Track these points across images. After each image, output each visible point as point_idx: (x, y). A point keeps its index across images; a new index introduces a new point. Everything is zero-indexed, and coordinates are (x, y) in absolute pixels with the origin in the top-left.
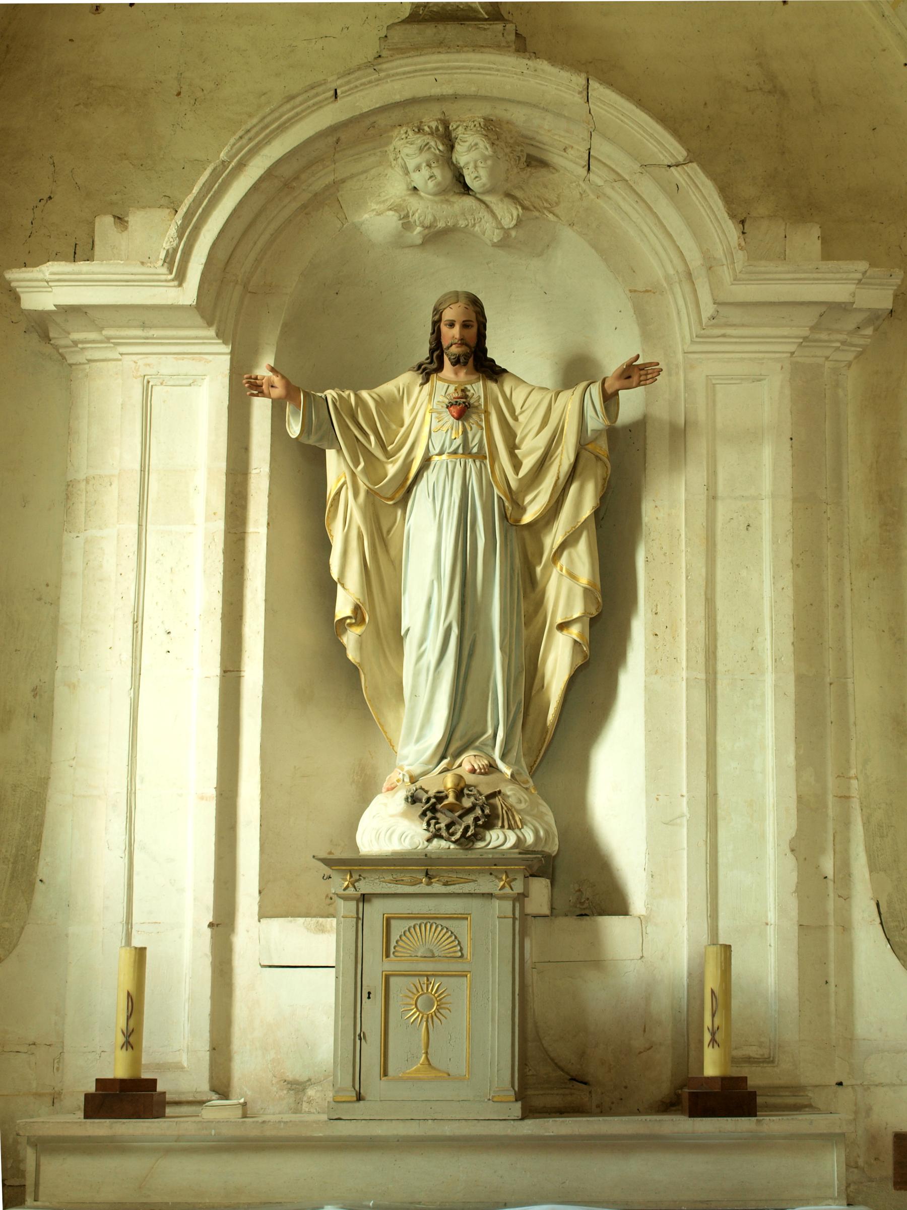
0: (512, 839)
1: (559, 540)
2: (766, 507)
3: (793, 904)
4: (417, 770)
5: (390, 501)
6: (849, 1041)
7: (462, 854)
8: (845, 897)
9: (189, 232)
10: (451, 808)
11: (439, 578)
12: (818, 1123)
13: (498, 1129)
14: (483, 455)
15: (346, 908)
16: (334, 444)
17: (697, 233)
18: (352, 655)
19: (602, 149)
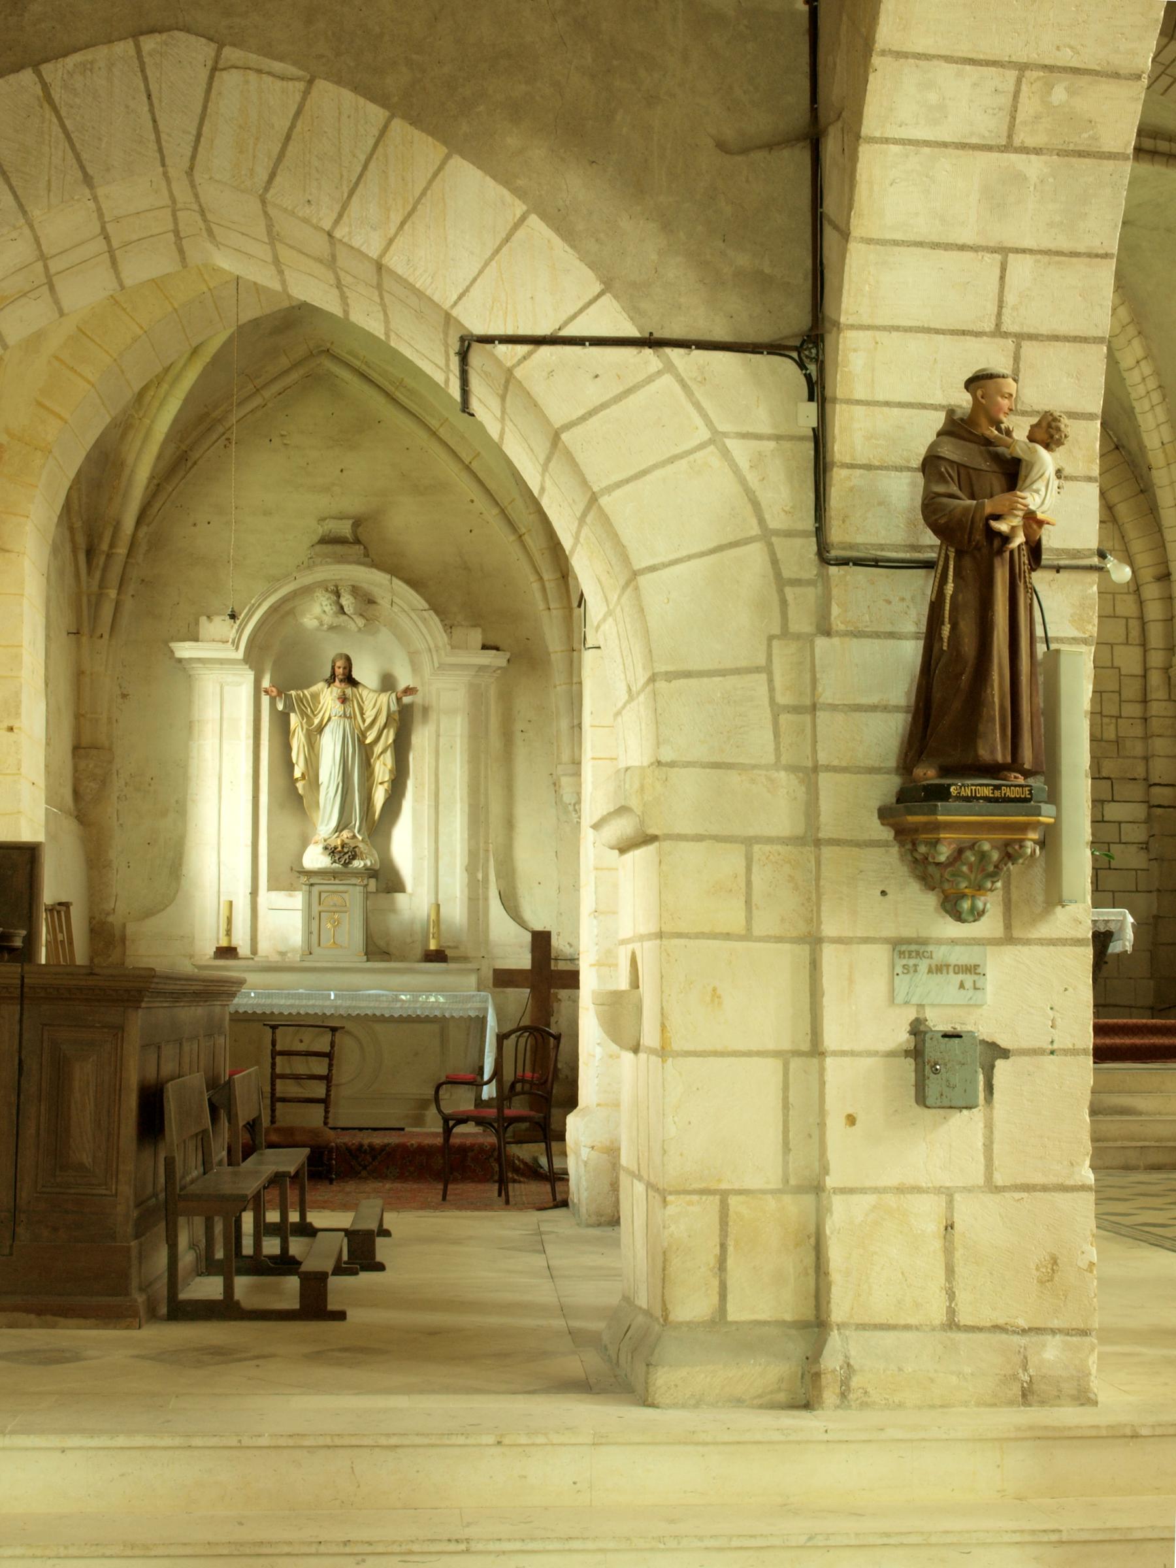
0: (362, 864)
3: (466, 890)
4: (326, 836)
5: (314, 734)
6: (487, 942)
7: (345, 870)
8: (486, 888)
12: (469, 966)
15: (305, 888)
16: (294, 711)
18: (300, 791)
19: (396, 600)
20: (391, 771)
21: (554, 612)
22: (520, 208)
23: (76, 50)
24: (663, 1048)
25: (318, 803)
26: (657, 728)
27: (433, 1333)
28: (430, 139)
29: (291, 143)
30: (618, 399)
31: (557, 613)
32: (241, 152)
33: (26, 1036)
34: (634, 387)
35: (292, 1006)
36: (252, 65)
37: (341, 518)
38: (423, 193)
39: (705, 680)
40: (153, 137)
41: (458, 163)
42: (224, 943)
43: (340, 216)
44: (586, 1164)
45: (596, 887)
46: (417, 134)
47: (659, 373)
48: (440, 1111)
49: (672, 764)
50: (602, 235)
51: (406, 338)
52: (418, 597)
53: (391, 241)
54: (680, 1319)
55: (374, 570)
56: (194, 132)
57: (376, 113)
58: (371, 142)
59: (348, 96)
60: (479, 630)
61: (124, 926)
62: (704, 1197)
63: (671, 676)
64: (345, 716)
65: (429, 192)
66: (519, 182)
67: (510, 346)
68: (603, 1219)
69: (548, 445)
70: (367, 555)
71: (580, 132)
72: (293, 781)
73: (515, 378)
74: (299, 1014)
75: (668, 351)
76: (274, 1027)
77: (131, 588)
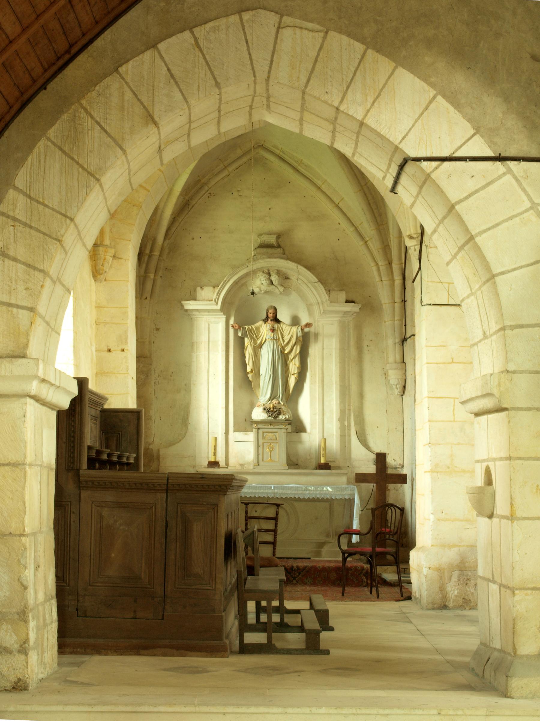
0: (284, 417)
1: (292, 357)
2: (334, 351)
3: (339, 431)
4: (264, 403)
6: (350, 458)
8: (349, 430)
9: (219, 294)
10: (272, 411)
11: (268, 364)
12: (342, 471)
13: (284, 471)
14: (277, 340)
16: (247, 337)
17: (320, 297)
18: (250, 379)
19: (300, 277)
20: (298, 368)
21: (385, 282)
22: (432, 92)
23: (211, 21)
24: (512, 516)
25: (259, 384)
26: (506, 354)
27: (378, 661)
28: (387, 59)
29: (317, 63)
30: (483, 188)
31: (386, 283)
32: (293, 69)
33: (169, 509)
34: (491, 181)
35: (251, 493)
36: (297, 25)
37: (270, 234)
38: (384, 87)
39: (531, 329)
40: (249, 63)
41: (401, 72)
42: (212, 460)
43: (343, 99)
44: (426, 577)
45: (430, 431)
46: (380, 57)
47: (504, 174)
48: (341, 549)
49: (514, 372)
50: (474, 105)
51: (366, 156)
52: (312, 275)
53: (368, 111)
54: (523, 653)
55: (289, 262)
56: (270, 60)
57: (359, 47)
58: (357, 61)
59: (345, 39)
60: (344, 292)
61: (159, 450)
62: (534, 592)
63: (512, 327)
64: (274, 339)
65: (387, 86)
66: (432, 80)
67: (429, 162)
68: (435, 606)
69: (446, 211)
70: (284, 254)
71: (462, 54)
72: (246, 374)
73: (431, 178)
74: (255, 497)
75: (508, 162)
76: (246, 504)
77: (160, 273)
